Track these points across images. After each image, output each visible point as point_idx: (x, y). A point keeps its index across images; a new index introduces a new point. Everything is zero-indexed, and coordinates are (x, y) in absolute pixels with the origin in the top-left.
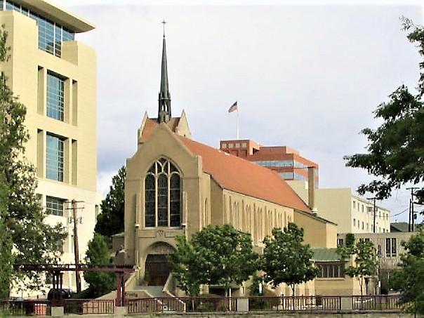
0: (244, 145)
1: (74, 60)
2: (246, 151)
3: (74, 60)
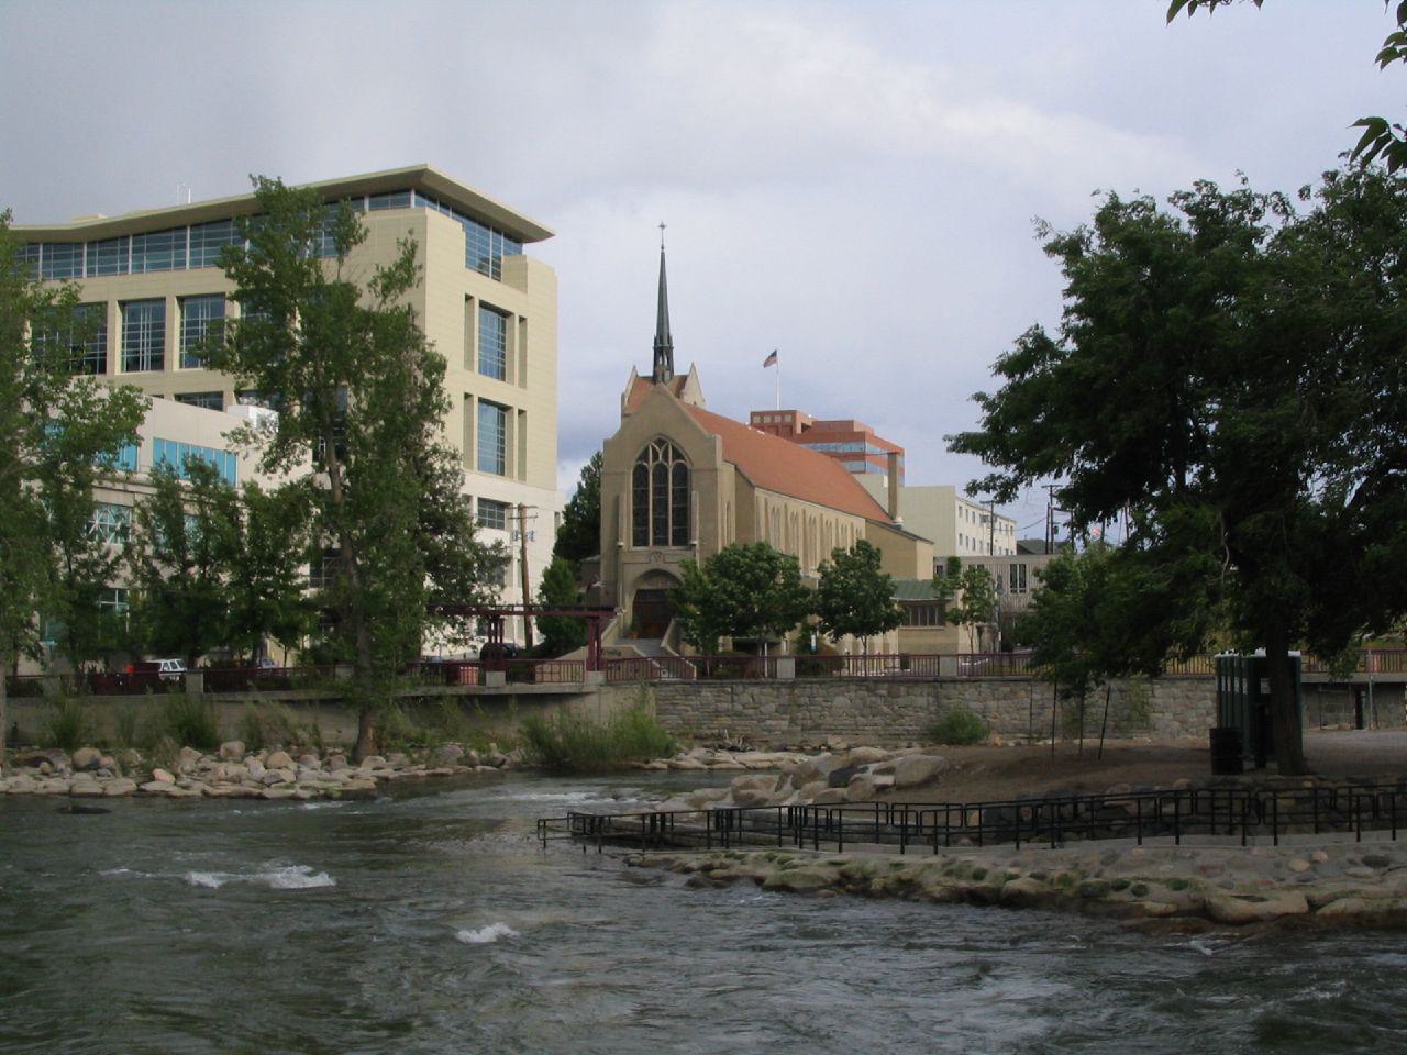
0: (788, 419)
1: (522, 286)
2: (791, 428)
3: (522, 286)
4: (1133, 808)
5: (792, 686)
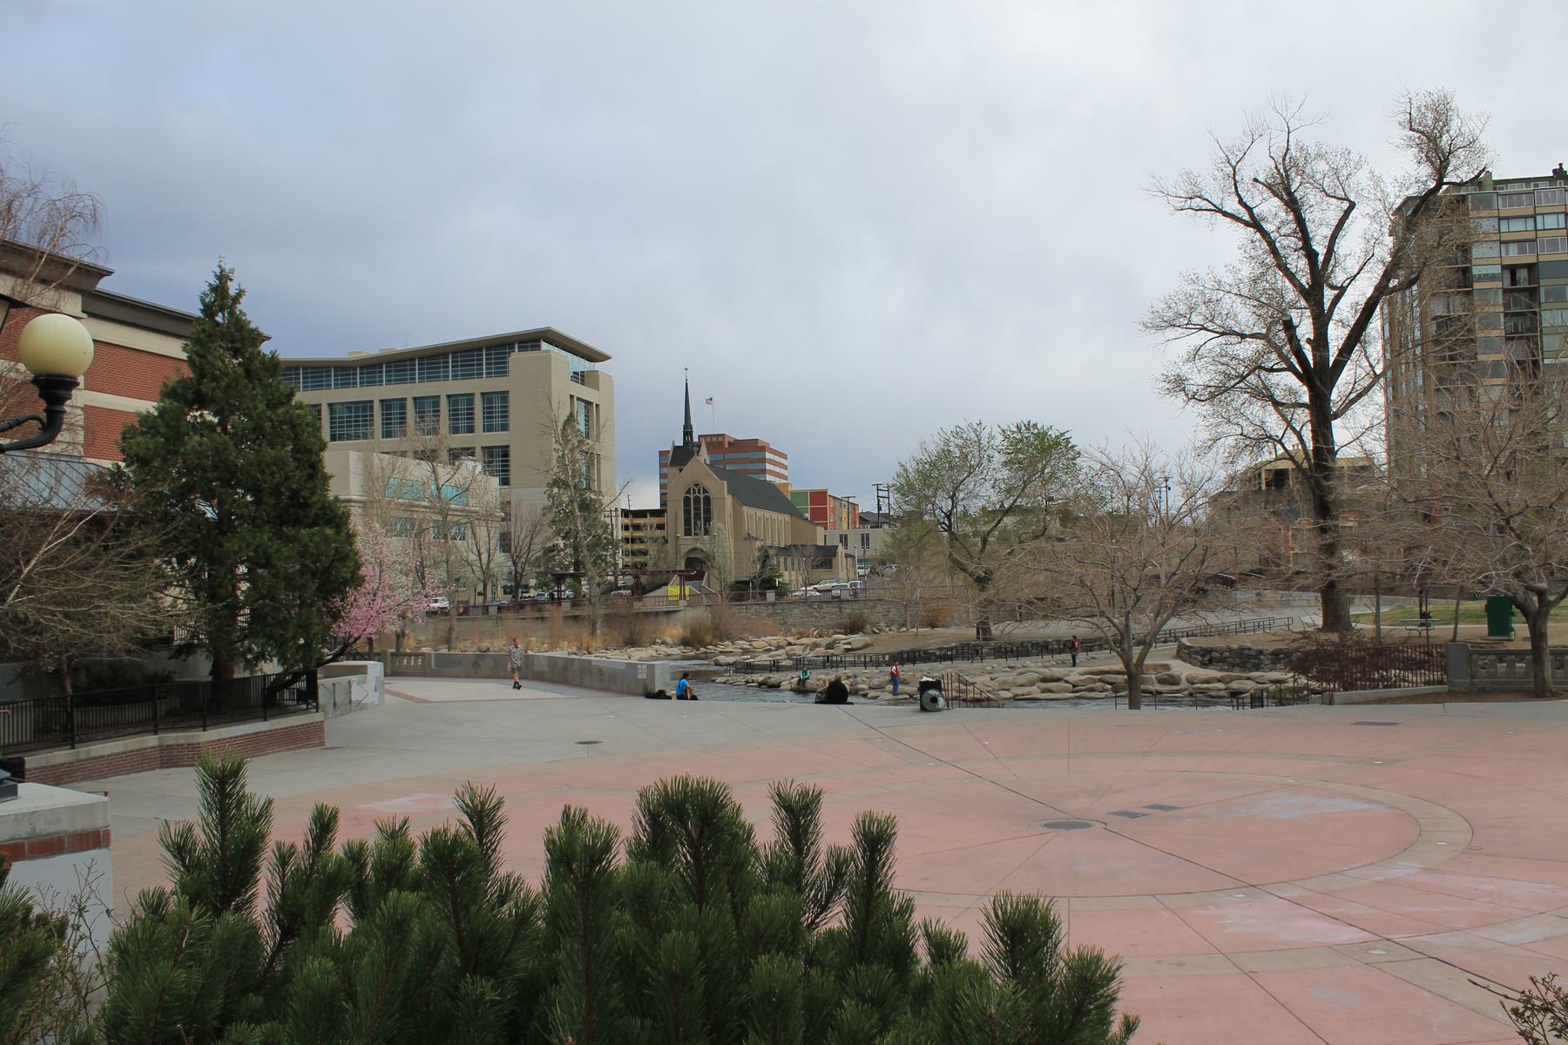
0: (720, 439)
1: (596, 388)
2: (722, 444)
3: (596, 388)
4: (938, 653)
5: (774, 604)
